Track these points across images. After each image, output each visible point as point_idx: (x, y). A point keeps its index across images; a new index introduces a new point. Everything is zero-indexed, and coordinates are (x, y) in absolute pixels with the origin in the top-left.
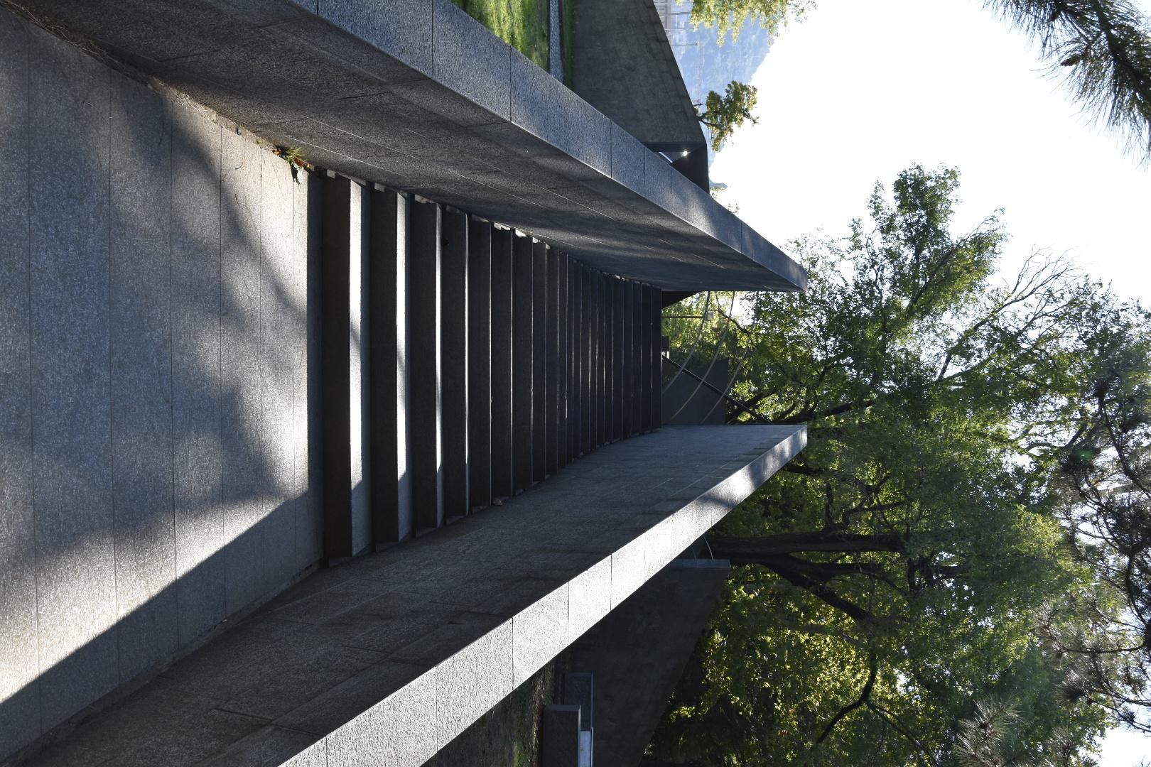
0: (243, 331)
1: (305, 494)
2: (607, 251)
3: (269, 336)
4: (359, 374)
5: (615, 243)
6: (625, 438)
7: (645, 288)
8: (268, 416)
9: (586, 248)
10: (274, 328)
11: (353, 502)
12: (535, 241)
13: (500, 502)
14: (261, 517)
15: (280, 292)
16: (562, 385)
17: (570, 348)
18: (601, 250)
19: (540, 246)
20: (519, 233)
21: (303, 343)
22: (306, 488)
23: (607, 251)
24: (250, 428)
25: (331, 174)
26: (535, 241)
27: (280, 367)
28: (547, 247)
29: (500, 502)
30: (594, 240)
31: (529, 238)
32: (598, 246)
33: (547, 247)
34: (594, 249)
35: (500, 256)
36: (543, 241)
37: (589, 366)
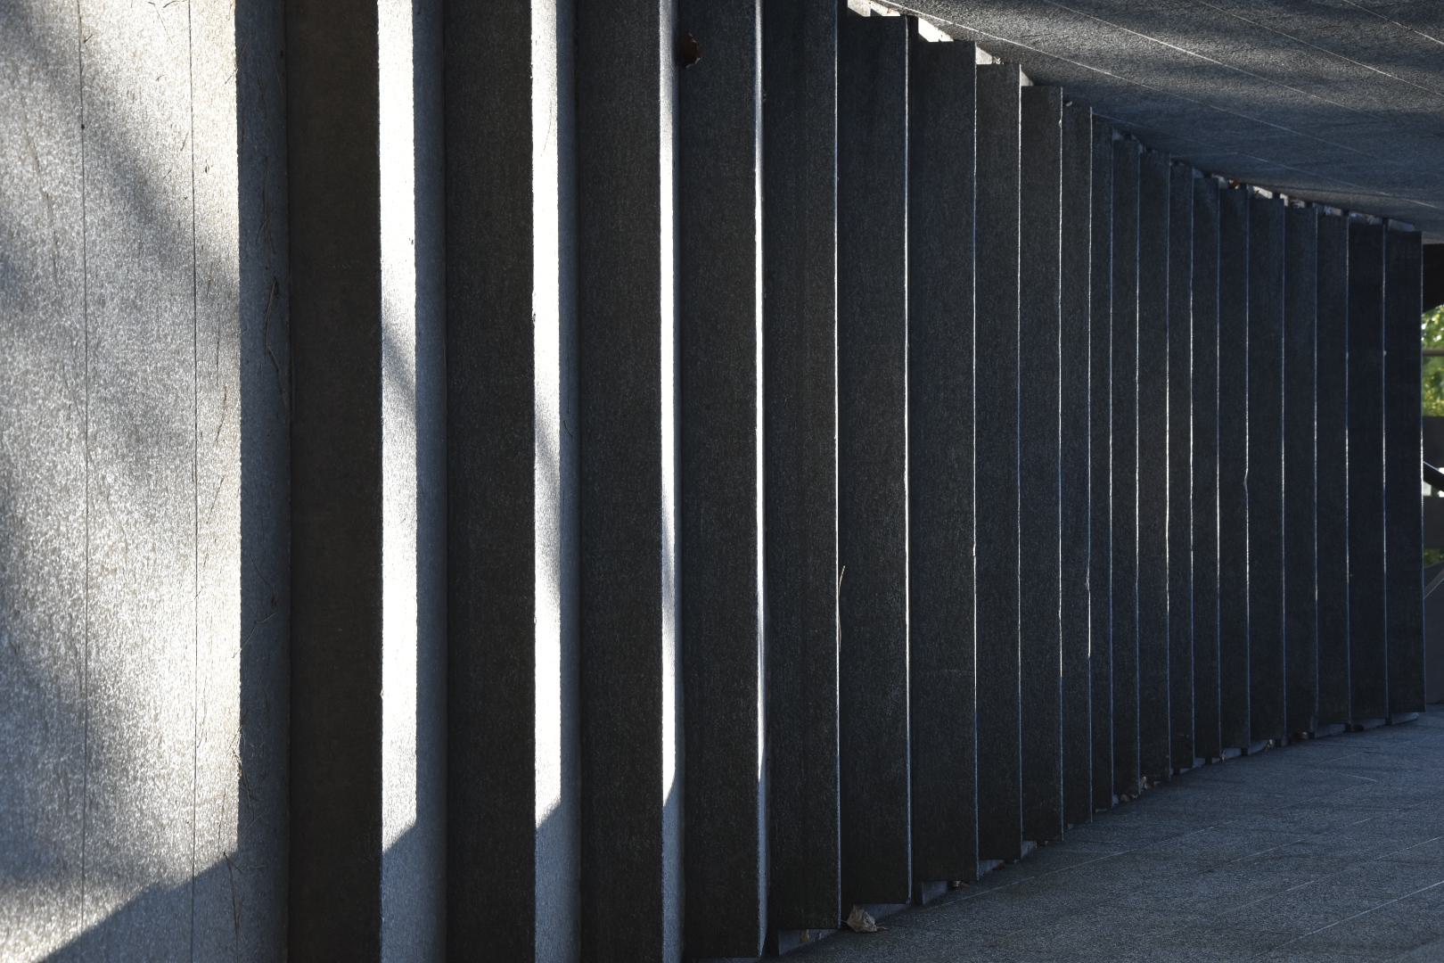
0: (25, 304)
1: (227, 863)
2: (1228, 89)
3: (115, 333)
4: (556, 614)
5: (1258, 57)
6: (1295, 740)
7: (1359, 229)
8: (109, 592)
9: (1157, 82)
10: (131, 307)
11: (388, 891)
12: (982, 58)
13: (870, 922)
14: (75, 929)
15: (137, 191)
16: (1039, 290)
17: (1099, 420)
18: (1207, 86)
19: (998, 77)
20: (930, 32)
21: (229, 365)
22: (229, 840)
23: (1228, 89)
24: (48, 626)
25: (985, 867)
26: (982, 58)
27: (146, 438)
28: (1023, 80)
29: (870, 922)
30: (1185, 49)
31: (961, 49)
32: (1199, 70)
33: (1023, 80)
34: (1184, 84)
35: (865, 105)
36: (1009, 57)
37: (1165, 482)
